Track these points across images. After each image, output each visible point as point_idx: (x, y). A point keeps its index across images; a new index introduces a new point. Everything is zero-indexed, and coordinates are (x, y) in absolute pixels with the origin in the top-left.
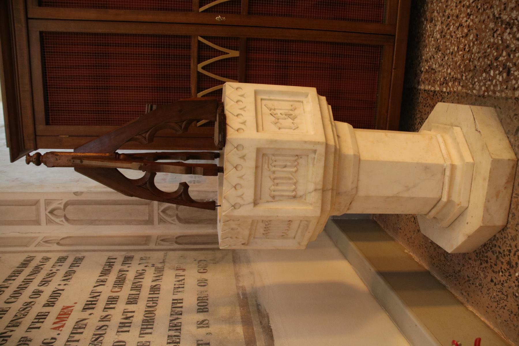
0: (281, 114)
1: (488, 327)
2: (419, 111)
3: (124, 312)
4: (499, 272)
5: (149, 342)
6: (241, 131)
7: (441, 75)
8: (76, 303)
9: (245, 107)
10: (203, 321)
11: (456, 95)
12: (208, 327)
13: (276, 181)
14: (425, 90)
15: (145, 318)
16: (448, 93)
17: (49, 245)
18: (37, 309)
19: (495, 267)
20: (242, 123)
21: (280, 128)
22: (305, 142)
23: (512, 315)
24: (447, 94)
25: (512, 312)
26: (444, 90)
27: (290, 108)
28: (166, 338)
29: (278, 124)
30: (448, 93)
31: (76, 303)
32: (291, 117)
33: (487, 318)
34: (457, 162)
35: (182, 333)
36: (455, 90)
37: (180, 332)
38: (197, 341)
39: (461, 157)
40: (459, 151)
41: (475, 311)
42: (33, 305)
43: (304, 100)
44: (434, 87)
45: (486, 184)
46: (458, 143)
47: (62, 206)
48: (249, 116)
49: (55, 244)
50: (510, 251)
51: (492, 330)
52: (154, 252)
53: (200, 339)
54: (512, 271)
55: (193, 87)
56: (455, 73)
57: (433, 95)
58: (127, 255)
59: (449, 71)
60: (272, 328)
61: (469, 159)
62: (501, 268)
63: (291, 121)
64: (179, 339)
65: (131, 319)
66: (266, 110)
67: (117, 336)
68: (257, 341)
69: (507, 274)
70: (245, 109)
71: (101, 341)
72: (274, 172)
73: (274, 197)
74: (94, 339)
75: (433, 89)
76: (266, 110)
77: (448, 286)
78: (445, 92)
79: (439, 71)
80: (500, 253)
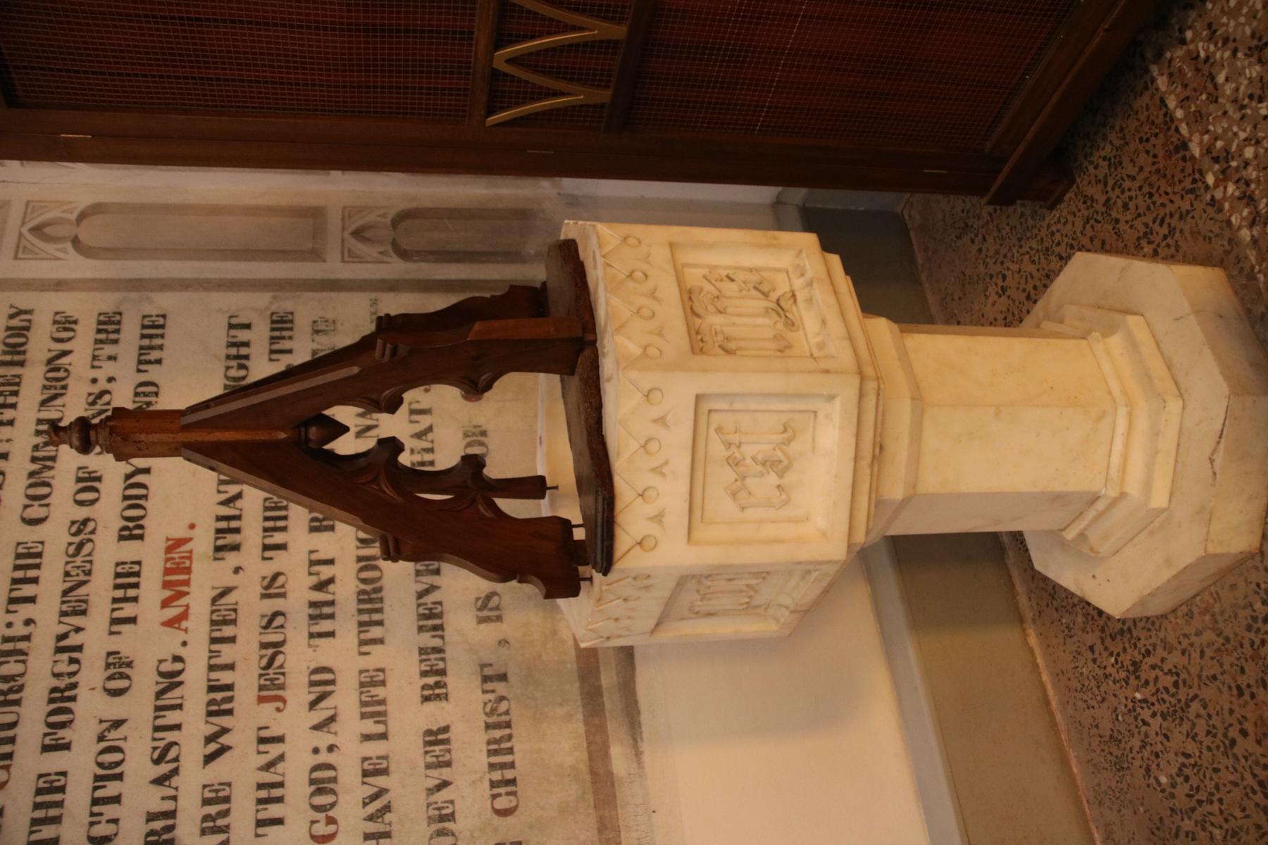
0: (754, 459)
1: (1047, 703)
2: (1122, 129)
3: (313, 563)
4: (1111, 654)
5: (382, 670)
7: (1225, 131)
8: (192, 526)
9: (666, 463)
10: (489, 597)
11: (1227, 234)
12: (499, 619)
14: (1163, 102)
15: (363, 587)
16: (1213, 198)
17: (51, 248)
18: (108, 552)
19: (1109, 639)
20: (652, 519)
21: (743, 509)
23: (1094, 731)
24: (1208, 197)
25: (1097, 726)
26: (1210, 179)
28: (416, 657)
30: (1213, 198)
31: (192, 526)
33: (1054, 685)
34: (1133, 488)
35: (447, 638)
36: (1233, 219)
37: (442, 637)
38: (483, 666)
39: (1148, 485)
40: (1150, 467)
41: (1037, 652)
42: (93, 532)
44: (1191, 134)
45: (1167, 575)
46: (1156, 452)
47: (73, 217)
48: (671, 494)
49: (69, 245)
50: (1148, 653)
51: (1051, 713)
52: (344, 296)
53: (486, 661)
54: (1133, 681)
55: (482, 38)
56: (1258, 181)
57: (1177, 150)
58: (274, 308)
59: (1249, 152)
61: (1159, 499)
62: (1118, 655)
63: (773, 479)
64: (443, 659)
65: (331, 587)
66: (717, 449)
67: (310, 651)
68: (602, 669)
69: (1123, 674)
71: (281, 666)
74: (264, 662)
75: (1184, 129)
77: (1011, 554)
78: (1207, 187)
79: (1225, 113)
80: (1129, 630)
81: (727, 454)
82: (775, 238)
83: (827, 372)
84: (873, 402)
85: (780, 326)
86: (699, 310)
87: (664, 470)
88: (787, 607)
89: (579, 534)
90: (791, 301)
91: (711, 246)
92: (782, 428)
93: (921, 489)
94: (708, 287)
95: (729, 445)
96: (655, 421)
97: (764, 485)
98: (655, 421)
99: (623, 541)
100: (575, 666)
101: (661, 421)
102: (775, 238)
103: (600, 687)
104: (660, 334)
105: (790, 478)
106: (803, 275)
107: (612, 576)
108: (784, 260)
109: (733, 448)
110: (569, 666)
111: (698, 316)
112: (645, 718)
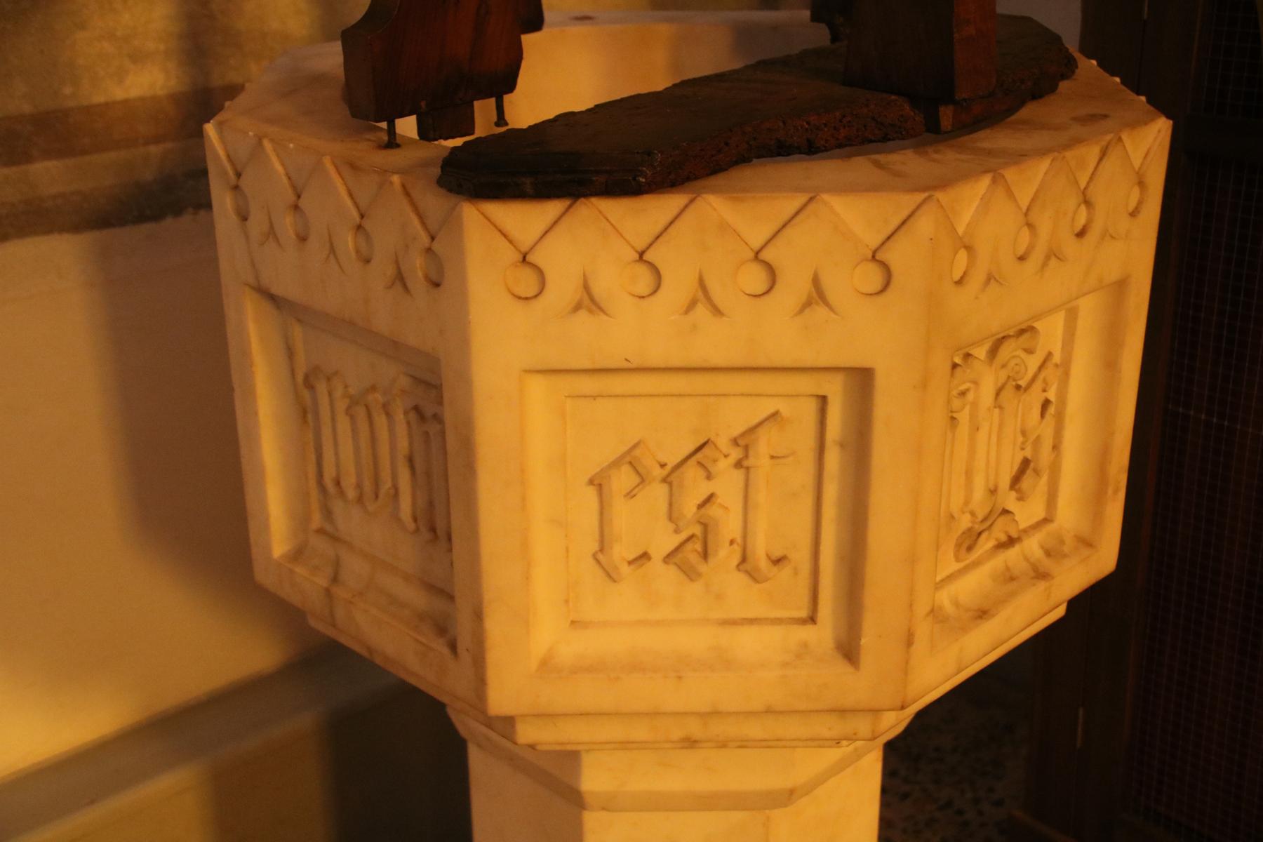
6: (527, 283)
9: (717, 311)
13: (361, 412)
21: (598, 483)
22: (478, 615)
27: (761, 547)
29: (623, 479)
32: (691, 553)
43: (823, 635)
60: (169, 222)
70: (701, 310)
72: (386, 409)
73: (309, 385)
76: (735, 416)
81: (723, 442)
82: (1116, 491)
83: (909, 641)
84: (826, 733)
85: (965, 522)
86: (1006, 352)
87: (701, 310)
88: (335, 579)
89: (483, 111)
90: (1003, 538)
91: (1111, 365)
92: (777, 554)
93: (592, 820)
94: (1033, 362)
95: (744, 442)
96: (816, 281)
97: (644, 522)
98: (816, 281)
99: (524, 219)
100: (71, 104)
101: (818, 295)
102: (1116, 491)
103: (28, 159)
104: (990, 278)
105: (665, 577)
106: (1048, 553)
107: (434, 202)
108: (1069, 516)
109: (736, 454)
110: (67, 90)
111: (993, 352)
112: (632, 444)
